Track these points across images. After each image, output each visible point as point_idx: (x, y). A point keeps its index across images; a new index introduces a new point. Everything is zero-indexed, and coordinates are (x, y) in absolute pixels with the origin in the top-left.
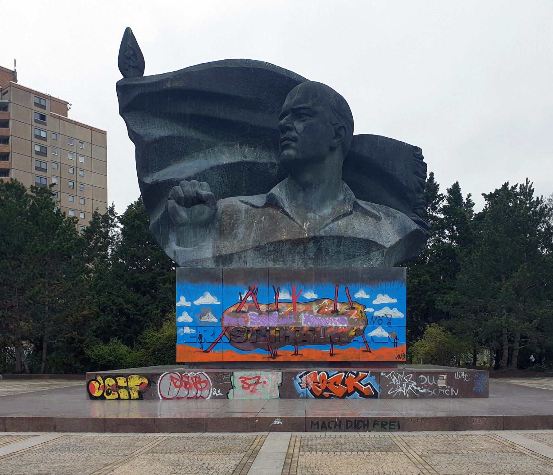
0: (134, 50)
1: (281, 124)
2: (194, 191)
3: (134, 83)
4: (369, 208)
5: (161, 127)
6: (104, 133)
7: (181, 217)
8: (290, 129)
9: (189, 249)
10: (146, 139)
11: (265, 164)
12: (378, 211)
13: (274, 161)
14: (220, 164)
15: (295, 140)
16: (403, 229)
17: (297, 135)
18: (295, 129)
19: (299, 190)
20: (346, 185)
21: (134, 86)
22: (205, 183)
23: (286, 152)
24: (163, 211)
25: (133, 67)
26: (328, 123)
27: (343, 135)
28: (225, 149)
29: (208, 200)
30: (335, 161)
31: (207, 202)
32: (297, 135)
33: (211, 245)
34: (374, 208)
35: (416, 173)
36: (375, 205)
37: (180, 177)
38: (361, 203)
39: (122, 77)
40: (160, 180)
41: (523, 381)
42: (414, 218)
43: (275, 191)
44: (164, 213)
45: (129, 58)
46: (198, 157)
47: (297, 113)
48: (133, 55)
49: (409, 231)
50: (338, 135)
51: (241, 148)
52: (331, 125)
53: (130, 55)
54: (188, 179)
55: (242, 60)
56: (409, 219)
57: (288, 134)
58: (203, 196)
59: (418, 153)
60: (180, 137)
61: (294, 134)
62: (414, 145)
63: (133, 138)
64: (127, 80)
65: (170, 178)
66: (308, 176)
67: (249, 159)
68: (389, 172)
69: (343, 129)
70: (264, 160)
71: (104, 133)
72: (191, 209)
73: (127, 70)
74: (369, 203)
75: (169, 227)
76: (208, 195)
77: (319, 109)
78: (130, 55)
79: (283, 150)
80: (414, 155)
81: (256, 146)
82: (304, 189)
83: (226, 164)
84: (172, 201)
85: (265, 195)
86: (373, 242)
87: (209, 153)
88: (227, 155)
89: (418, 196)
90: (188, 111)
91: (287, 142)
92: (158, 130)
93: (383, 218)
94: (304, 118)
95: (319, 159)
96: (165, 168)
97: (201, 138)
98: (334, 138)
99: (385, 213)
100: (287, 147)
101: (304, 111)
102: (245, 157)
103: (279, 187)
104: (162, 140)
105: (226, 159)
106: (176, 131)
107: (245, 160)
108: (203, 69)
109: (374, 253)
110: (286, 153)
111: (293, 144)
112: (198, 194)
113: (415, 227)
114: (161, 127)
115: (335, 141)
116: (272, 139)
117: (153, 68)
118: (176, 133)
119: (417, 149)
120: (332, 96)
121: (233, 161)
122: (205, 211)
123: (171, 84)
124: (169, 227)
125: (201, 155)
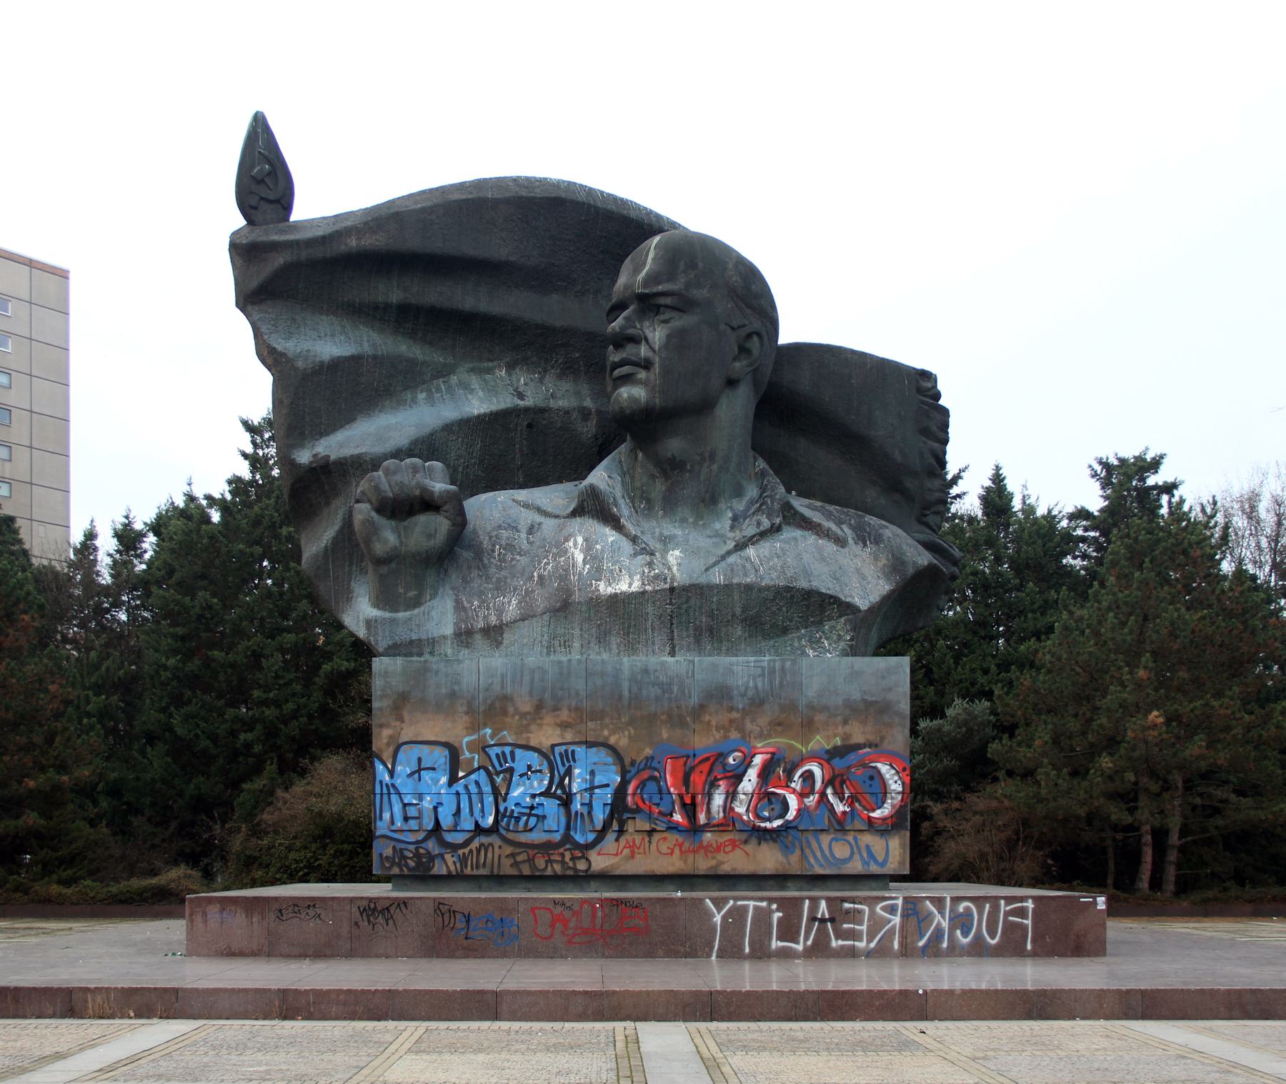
0: (270, 163)
1: (613, 329)
2: (414, 483)
3: (276, 238)
4: (816, 517)
5: (333, 336)
6: (63, 275)
7: (387, 541)
8: (635, 340)
9: (401, 615)
10: (300, 364)
11: (567, 412)
12: (839, 523)
13: (588, 403)
14: (465, 416)
15: (647, 365)
16: (897, 564)
17: (650, 354)
18: (646, 340)
19: (653, 477)
20: (761, 464)
21: (274, 247)
22: (437, 465)
23: (625, 392)
24: (337, 528)
25: (271, 202)
26: (722, 327)
27: (756, 352)
28: (475, 381)
29: (446, 503)
30: (734, 412)
31: (445, 508)
32: (650, 354)
33: (450, 604)
34: (829, 516)
35: (925, 432)
36: (832, 508)
37: (378, 449)
38: (800, 504)
39: (241, 222)
40: (333, 457)
41: (1196, 925)
42: (921, 537)
43: (599, 477)
44: (340, 532)
45: (260, 182)
46: (414, 400)
47: (648, 304)
48: (269, 174)
49: (911, 571)
50: (743, 350)
51: (510, 375)
52: (729, 331)
53: (263, 177)
54: (398, 454)
55: (515, 180)
56: (910, 541)
57: (628, 351)
58: (436, 495)
59: (929, 385)
60: (375, 357)
61: (643, 351)
62: (919, 366)
63: (270, 361)
64: (257, 230)
65: (357, 451)
66: (674, 445)
67: (528, 402)
68: (856, 429)
69: (755, 339)
70: (563, 403)
71: (63, 275)
72: (406, 523)
73: (255, 208)
74: (819, 504)
75: (351, 565)
76: (448, 491)
77: (702, 293)
78: (263, 177)
79: (616, 387)
80: (920, 391)
81: (545, 371)
82: (665, 474)
83: (478, 416)
84: (364, 507)
85: (568, 486)
86: (831, 597)
87: (438, 390)
88: (481, 393)
89: (929, 485)
90: (395, 297)
91: (626, 369)
92: (327, 343)
93: (851, 541)
94: (666, 316)
95: (704, 407)
96: (341, 427)
97: (420, 357)
98: (735, 359)
99: (853, 528)
100: (627, 379)
101: (663, 301)
102: (521, 396)
103: (606, 469)
104: (335, 365)
105: (477, 404)
106: (366, 345)
107: (521, 403)
108: (429, 204)
109: (832, 623)
110: (625, 395)
111: (642, 375)
112: (424, 489)
113: (924, 558)
114: (333, 336)
115: (737, 364)
116: (588, 356)
117: (318, 199)
118: (367, 349)
119: (926, 375)
120: (730, 266)
121: (494, 408)
122: (435, 527)
123: (359, 239)
124: (351, 565)
125: (422, 396)
